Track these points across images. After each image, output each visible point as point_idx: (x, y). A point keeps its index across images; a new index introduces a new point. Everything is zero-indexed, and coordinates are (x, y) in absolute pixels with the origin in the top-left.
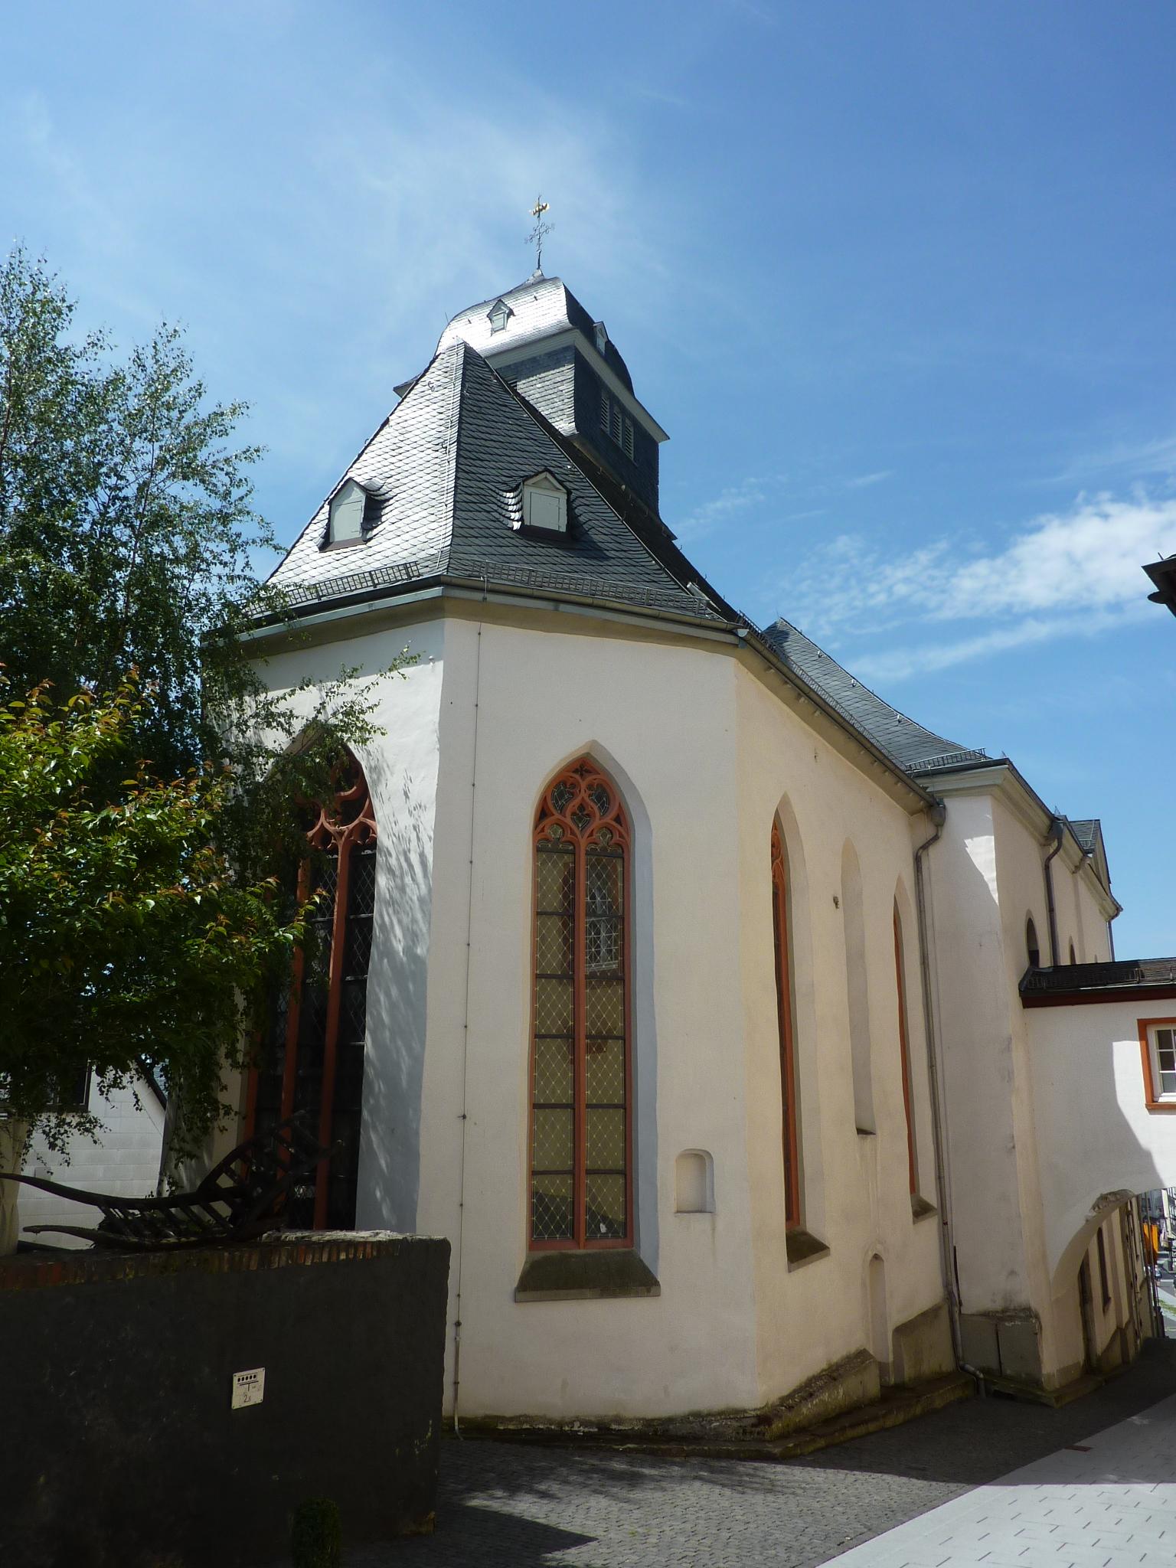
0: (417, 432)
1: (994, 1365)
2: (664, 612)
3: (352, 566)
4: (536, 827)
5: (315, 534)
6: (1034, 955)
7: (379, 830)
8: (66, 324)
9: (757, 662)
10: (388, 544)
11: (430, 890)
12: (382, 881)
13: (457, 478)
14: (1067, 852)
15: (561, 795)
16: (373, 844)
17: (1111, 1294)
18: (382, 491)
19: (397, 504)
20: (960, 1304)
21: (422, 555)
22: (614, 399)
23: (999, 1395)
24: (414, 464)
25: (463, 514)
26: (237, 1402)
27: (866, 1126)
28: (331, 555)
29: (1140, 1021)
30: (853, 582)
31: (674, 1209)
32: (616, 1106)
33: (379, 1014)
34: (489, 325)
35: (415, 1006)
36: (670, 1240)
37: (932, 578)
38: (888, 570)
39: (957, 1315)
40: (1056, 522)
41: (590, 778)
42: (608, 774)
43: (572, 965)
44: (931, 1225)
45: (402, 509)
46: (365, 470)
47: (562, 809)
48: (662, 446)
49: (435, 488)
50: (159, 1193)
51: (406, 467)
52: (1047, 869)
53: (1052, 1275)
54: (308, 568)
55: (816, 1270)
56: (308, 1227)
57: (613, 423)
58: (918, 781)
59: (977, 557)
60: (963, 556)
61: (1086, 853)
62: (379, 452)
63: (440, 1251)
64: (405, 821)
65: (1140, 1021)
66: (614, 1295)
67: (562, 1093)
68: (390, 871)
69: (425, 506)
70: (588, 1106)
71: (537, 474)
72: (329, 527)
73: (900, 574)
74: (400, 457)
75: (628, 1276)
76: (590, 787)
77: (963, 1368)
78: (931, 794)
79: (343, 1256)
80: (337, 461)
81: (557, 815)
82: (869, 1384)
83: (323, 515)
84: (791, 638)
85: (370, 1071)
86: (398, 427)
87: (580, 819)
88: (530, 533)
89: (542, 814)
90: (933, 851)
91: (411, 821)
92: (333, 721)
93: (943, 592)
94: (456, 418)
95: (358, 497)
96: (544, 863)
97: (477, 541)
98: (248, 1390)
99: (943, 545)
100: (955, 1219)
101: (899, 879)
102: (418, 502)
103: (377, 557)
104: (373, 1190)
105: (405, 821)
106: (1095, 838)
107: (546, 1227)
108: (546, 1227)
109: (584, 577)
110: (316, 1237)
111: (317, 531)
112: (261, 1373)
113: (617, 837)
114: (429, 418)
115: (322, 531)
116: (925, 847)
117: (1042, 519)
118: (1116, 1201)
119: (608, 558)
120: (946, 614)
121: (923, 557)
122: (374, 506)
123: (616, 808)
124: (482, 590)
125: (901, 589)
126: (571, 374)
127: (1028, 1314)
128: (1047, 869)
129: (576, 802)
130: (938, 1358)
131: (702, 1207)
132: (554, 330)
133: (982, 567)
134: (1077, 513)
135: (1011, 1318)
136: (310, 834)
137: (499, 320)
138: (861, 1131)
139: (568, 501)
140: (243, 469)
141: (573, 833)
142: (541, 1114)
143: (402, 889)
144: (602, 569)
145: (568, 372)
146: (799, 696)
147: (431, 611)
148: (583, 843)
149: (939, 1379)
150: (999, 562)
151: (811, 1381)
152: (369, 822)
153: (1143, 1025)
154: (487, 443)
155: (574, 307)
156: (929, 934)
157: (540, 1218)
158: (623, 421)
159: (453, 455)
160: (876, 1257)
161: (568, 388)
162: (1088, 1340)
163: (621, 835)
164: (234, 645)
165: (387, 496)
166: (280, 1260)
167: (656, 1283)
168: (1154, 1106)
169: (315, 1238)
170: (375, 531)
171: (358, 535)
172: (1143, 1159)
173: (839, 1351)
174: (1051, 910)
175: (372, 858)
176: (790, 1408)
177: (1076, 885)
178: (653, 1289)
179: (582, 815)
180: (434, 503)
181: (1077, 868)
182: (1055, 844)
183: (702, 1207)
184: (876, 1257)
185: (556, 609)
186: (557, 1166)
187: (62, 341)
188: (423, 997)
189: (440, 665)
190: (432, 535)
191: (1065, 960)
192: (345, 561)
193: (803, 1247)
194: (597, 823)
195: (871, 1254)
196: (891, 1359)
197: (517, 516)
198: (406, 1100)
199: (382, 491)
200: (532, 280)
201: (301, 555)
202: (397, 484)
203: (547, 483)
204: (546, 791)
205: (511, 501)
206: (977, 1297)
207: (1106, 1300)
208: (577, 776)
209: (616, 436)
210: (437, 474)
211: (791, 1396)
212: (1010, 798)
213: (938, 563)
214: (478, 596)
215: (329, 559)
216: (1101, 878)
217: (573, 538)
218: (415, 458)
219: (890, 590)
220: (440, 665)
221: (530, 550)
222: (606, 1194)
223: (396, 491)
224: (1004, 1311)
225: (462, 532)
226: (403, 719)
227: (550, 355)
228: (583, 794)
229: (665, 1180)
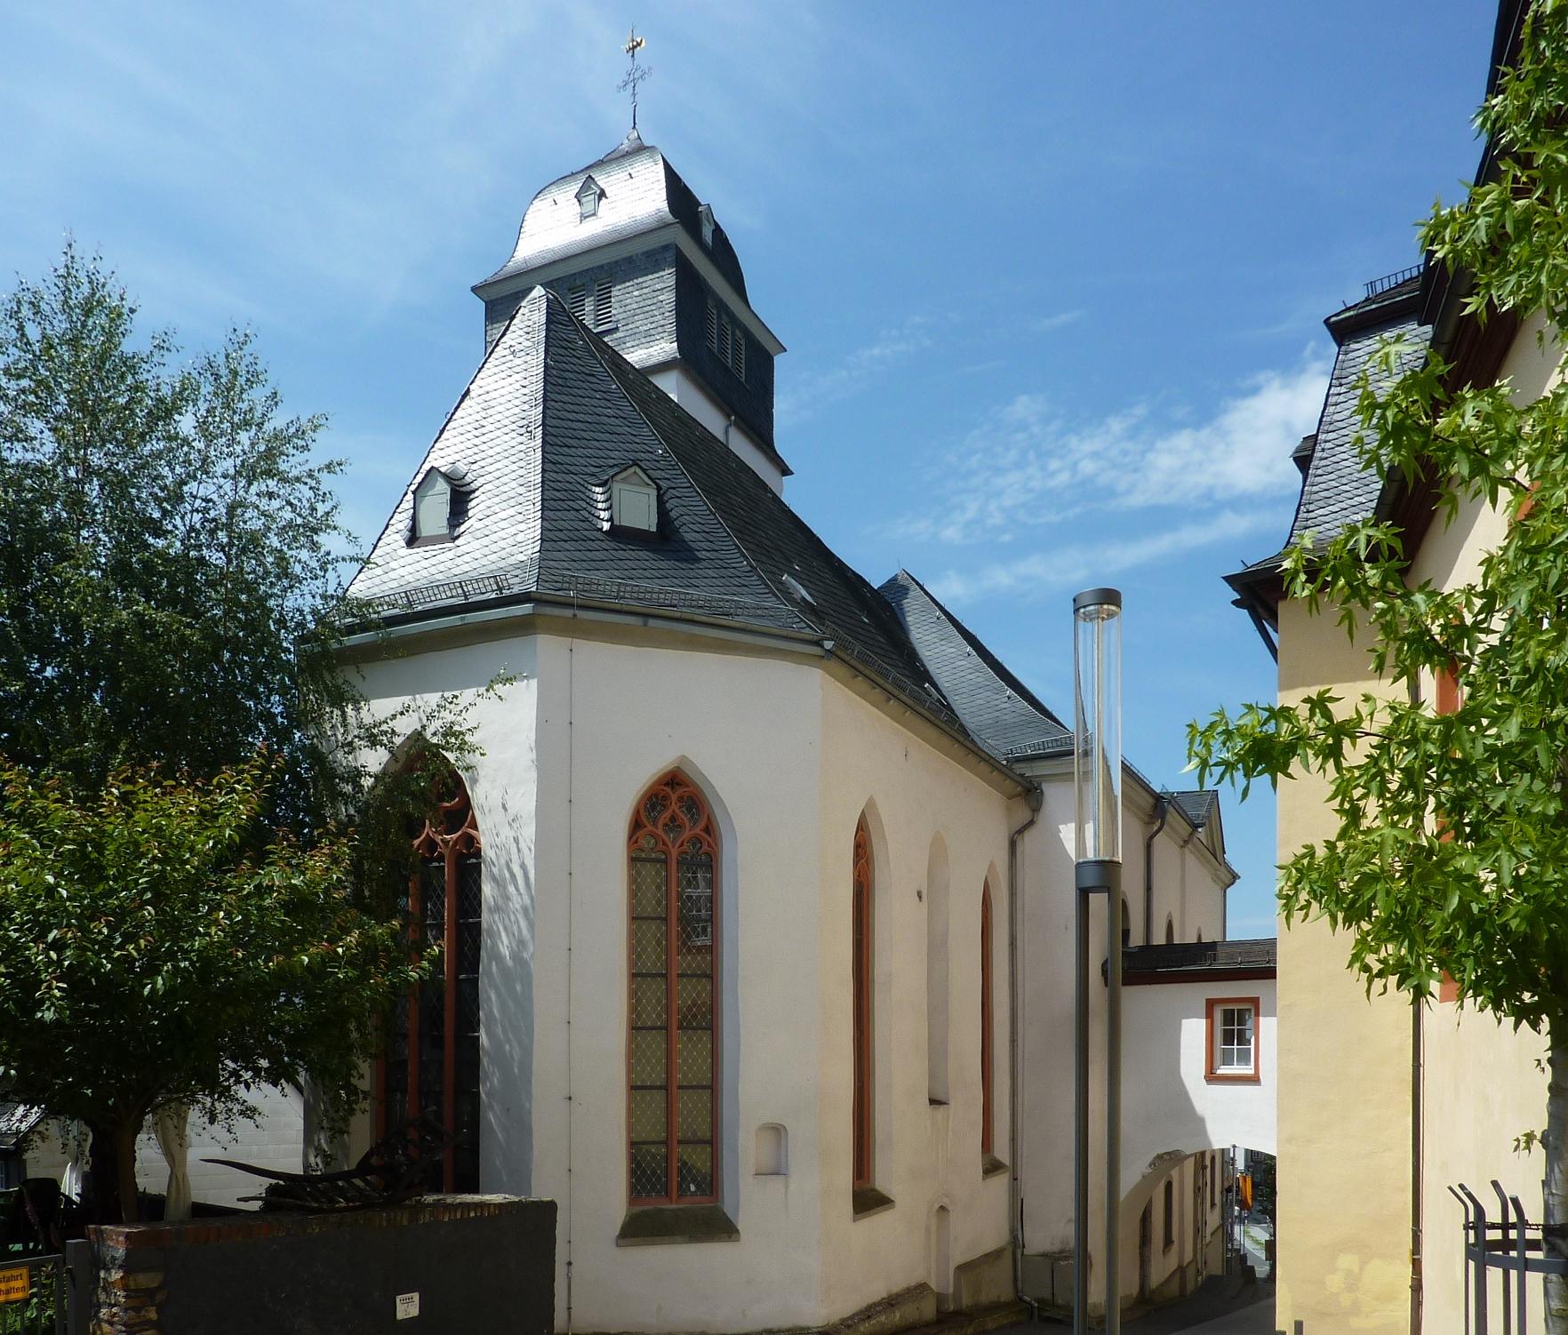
0: (500, 408)
1: (1048, 1296)
2: (755, 623)
3: (441, 568)
4: (630, 838)
5: (401, 526)
6: (1126, 934)
7: (482, 840)
8: (128, 326)
9: (843, 671)
10: (476, 544)
11: (532, 899)
12: (487, 889)
13: (544, 471)
14: (1171, 826)
15: (653, 808)
16: (478, 854)
17: (1175, 1236)
18: (467, 479)
19: (483, 497)
21: (512, 560)
22: (722, 307)
23: (1048, 1320)
24: (498, 449)
25: (551, 514)
26: (400, 1315)
27: (941, 1097)
28: (419, 552)
30: (1031, 456)
32: (704, 1087)
33: (491, 1012)
34: (577, 208)
35: (523, 1007)
36: (748, 1197)
37: (1125, 453)
38: (1073, 441)
40: (1276, 383)
41: (680, 791)
42: (696, 786)
43: (668, 963)
44: (1001, 1181)
45: (488, 503)
46: (447, 451)
47: (655, 824)
48: (779, 361)
49: (521, 481)
50: (307, 1165)
51: (491, 452)
54: (397, 572)
55: (880, 1221)
56: (439, 1191)
57: (722, 338)
58: (1016, 766)
59: (1179, 426)
60: (1168, 426)
61: (1195, 827)
62: (461, 430)
63: (548, 1210)
64: (507, 833)
66: (700, 1240)
67: (658, 1077)
68: (494, 879)
69: (512, 502)
70: (680, 1087)
72: (414, 518)
73: (1087, 447)
74: (484, 439)
75: (714, 1225)
76: (680, 799)
80: (425, 477)
81: (650, 828)
82: (928, 1310)
83: (408, 503)
84: (911, 594)
85: (485, 1061)
86: (480, 400)
88: (620, 534)
89: (636, 825)
90: (1027, 834)
91: (512, 834)
92: (435, 740)
93: (1136, 471)
94: (540, 395)
95: (442, 487)
96: (639, 873)
98: (408, 1307)
99: (1141, 410)
100: (1025, 1173)
101: (992, 866)
102: (504, 497)
103: (467, 558)
104: (491, 1158)
105: (507, 833)
106: (1208, 811)
107: (644, 1188)
108: (644, 1188)
110: (450, 1199)
111: (402, 522)
112: (416, 1296)
113: (705, 847)
114: (511, 379)
115: (408, 523)
116: (1020, 831)
117: (1261, 377)
119: (698, 560)
120: (1137, 500)
121: (1116, 425)
124: (571, 605)
125: (1088, 467)
126: (672, 281)
130: (998, 1287)
131: (778, 1170)
132: (654, 225)
133: (1183, 440)
134: (1302, 371)
135: (1066, 1258)
136: (416, 842)
137: (589, 200)
138: (934, 1102)
139: (660, 497)
140: (327, 482)
142: (638, 1095)
143: (507, 898)
144: (692, 574)
145: (665, 279)
147: (522, 627)
148: (674, 852)
149: (996, 1307)
150: (1205, 434)
151: (875, 1305)
152: (473, 832)
153: (1211, 1004)
154: (574, 425)
155: (677, 191)
156: (1019, 916)
157: (638, 1180)
159: (539, 442)
160: (942, 1208)
161: (669, 297)
162: (1144, 1277)
164: (326, 653)
165: (473, 486)
166: (425, 1218)
167: (737, 1231)
168: (1212, 1077)
169: (449, 1201)
170: (462, 528)
171: (446, 531)
172: (1198, 1124)
173: (899, 1283)
174: (1149, 888)
175: (477, 868)
176: (849, 1327)
177: (1183, 859)
179: (674, 825)
180: (521, 499)
181: (1186, 842)
182: (1158, 823)
183: (778, 1170)
184: (942, 1208)
186: (653, 1137)
187: (127, 346)
188: (530, 998)
190: (520, 537)
191: (1159, 939)
192: (433, 561)
193: (868, 1200)
194: (687, 834)
195: (937, 1206)
196: (951, 1290)
197: (604, 515)
198: (519, 1084)
199: (467, 479)
200: (626, 146)
201: (388, 549)
202: (482, 472)
203: (635, 479)
204: (639, 803)
205: (600, 498)
207: (1168, 1241)
208: (668, 789)
209: (723, 351)
210: (522, 464)
211: (851, 1318)
213: (1133, 433)
214: (568, 613)
215: (417, 557)
216: (1216, 851)
217: (664, 540)
218: (497, 415)
219: (1074, 468)
221: (620, 554)
222: (698, 1158)
223: (481, 480)
224: (1061, 1252)
225: (550, 535)
226: (501, 732)
227: (649, 254)
229: (745, 1148)
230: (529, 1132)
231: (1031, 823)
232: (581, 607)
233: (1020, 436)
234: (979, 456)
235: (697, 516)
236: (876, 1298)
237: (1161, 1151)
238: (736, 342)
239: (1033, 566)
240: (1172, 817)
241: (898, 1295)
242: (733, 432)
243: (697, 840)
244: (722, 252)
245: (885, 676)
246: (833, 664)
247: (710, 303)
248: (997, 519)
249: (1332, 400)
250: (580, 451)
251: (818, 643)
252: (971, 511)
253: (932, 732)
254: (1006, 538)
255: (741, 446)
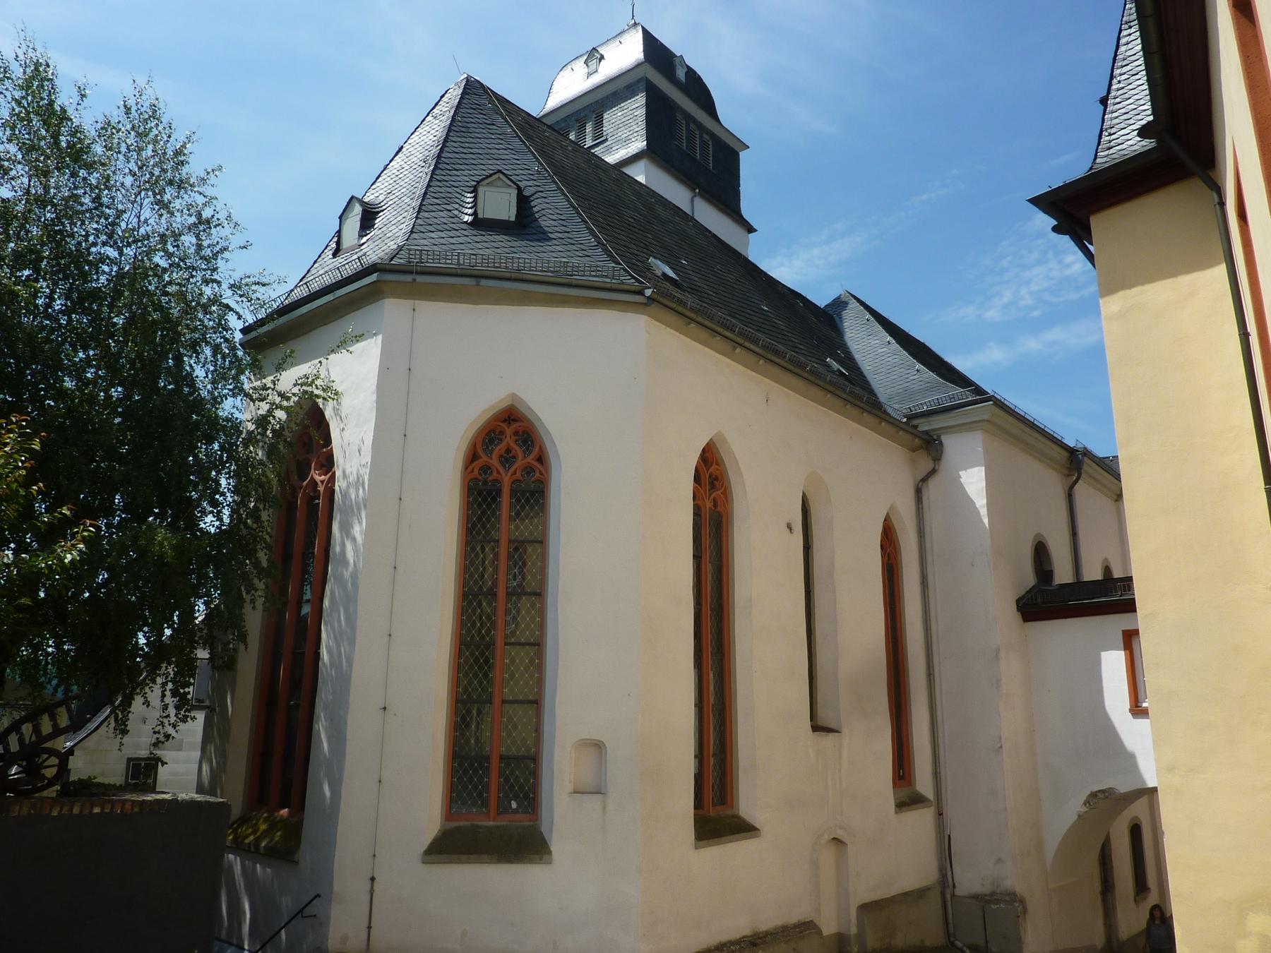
4: (466, 468)
20: (954, 886)
22: (700, 126)
29: (1124, 632)
30: (1050, 255)
31: (570, 788)
34: (586, 70)
39: (948, 897)
41: (514, 426)
44: (922, 819)
48: (743, 155)
52: (1070, 496)
53: (1049, 863)
57: (691, 139)
58: (915, 422)
65: (1124, 632)
71: (491, 175)
75: (527, 845)
76: (516, 433)
77: (953, 944)
78: (927, 432)
79: (97, 810)
87: (507, 461)
88: (479, 223)
89: (472, 456)
90: (932, 483)
97: (432, 235)
100: (950, 810)
109: (522, 254)
113: (537, 474)
116: (925, 480)
118: (1106, 803)
122: (369, 216)
123: (537, 449)
124: (411, 272)
127: (1012, 898)
128: (1070, 496)
129: (503, 445)
135: (997, 902)
137: (593, 64)
138: (817, 728)
141: (498, 472)
146: (735, 348)
147: (372, 295)
155: (651, 43)
158: (701, 137)
160: (837, 841)
163: (541, 473)
167: (550, 852)
174: (1074, 534)
178: (545, 857)
185: (478, 284)
189: (380, 337)
194: (519, 463)
196: (854, 930)
203: (500, 183)
206: (969, 880)
208: (504, 425)
212: (1008, 433)
214: (408, 278)
220: (380, 337)
224: (992, 894)
228: (509, 440)
230: (345, 739)
231: (933, 472)
232: (417, 273)
233: (1041, 241)
234: (1009, 258)
235: (553, 207)
236: (735, 935)
237: (1096, 789)
238: (704, 143)
239: (1056, 334)
240: (1088, 466)
241: (767, 934)
242: (698, 201)
243: (529, 470)
244: (696, 88)
245: (756, 342)
246: (654, 308)
247: (679, 116)
248: (1029, 301)
249: (1123, 41)
250: (466, 173)
251: (641, 293)
252: (1007, 296)
253: (801, 384)
254: (1036, 313)
255: (709, 217)
